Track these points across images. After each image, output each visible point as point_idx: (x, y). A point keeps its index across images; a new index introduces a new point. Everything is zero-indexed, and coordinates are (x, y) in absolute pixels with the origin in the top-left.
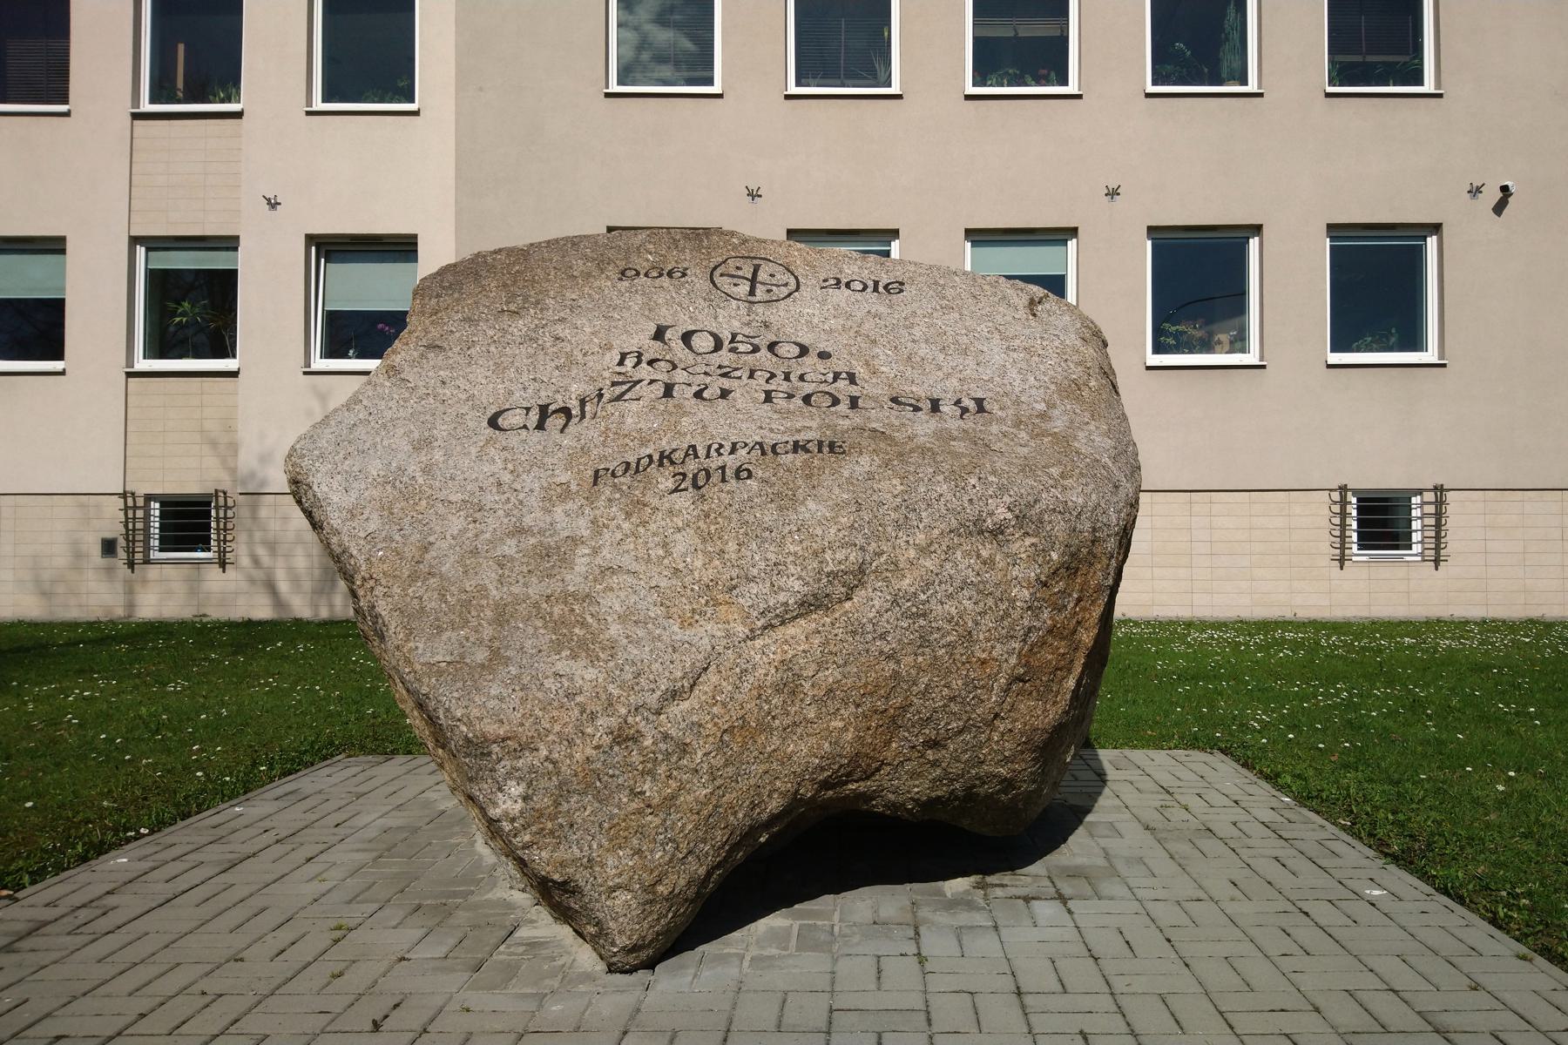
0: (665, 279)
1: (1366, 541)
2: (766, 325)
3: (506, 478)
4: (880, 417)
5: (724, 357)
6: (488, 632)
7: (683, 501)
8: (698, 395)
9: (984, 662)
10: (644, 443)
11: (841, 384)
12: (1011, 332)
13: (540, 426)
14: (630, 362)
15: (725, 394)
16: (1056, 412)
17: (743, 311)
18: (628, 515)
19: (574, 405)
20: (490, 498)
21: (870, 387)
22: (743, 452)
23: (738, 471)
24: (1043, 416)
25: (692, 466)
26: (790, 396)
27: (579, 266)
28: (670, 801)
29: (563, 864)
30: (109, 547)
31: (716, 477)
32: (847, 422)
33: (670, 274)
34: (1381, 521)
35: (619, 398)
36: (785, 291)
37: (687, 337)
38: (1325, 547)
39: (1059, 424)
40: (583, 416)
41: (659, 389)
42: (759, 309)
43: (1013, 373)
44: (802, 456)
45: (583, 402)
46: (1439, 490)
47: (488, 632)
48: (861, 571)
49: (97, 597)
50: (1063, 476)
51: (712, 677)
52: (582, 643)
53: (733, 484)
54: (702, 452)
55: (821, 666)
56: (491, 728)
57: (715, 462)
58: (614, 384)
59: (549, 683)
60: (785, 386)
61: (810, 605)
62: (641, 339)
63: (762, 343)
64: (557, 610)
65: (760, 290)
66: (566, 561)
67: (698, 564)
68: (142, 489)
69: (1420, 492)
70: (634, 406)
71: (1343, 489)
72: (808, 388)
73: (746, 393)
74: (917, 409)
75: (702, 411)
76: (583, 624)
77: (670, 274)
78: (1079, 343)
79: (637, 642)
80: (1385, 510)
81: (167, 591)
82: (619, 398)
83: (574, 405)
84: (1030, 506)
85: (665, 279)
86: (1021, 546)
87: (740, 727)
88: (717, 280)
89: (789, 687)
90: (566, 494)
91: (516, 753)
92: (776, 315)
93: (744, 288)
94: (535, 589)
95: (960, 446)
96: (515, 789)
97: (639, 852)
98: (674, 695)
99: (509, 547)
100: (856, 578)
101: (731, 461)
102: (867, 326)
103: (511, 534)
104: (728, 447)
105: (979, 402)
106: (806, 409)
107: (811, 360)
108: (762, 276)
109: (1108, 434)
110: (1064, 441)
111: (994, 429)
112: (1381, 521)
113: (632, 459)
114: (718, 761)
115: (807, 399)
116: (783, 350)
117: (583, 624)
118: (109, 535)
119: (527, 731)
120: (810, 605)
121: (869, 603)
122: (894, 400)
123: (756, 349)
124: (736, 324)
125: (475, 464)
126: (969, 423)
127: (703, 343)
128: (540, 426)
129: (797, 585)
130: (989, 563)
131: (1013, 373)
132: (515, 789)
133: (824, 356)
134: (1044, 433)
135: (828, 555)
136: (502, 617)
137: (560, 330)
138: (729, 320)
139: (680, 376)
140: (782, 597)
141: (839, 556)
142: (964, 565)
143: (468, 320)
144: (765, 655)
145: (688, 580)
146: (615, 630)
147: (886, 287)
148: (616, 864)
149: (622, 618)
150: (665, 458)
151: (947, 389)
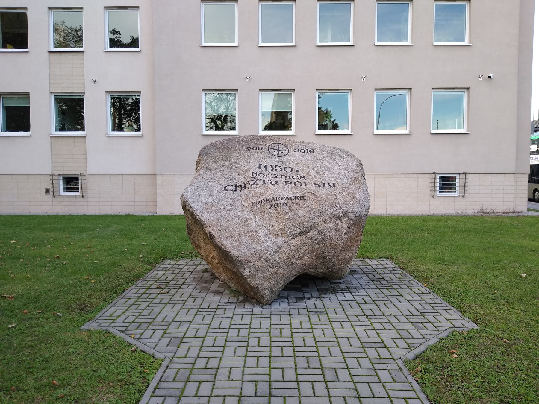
0: (257, 150)
1: (441, 190)
2: (283, 163)
3: (232, 203)
4: (313, 189)
5: (274, 172)
6: (237, 239)
7: (273, 210)
8: (271, 183)
9: (336, 245)
10: (261, 196)
11: (302, 179)
12: (340, 164)
13: (236, 190)
14: (255, 175)
15: (277, 182)
16: (351, 187)
17: (277, 159)
18: (261, 213)
19: (243, 185)
20: (229, 208)
21: (310, 181)
22: (284, 199)
23: (284, 204)
24: (348, 188)
25: (273, 202)
26: (291, 183)
27: (238, 147)
28: (276, 273)
29: (256, 284)
30: (47, 191)
31: (279, 206)
32: (305, 191)
33: (258, 149)
34: (447, 184)
35: (253, 184)
36: (286, 152)
37: (265, 167)
38: (428, 192)
39: (352, 190)
40: (245, 188)
41: (262, 182)
42: (281, 158)
43: (341, 176)
44: (297, 200)
45: (245, 184)
46: (465, 173)
47: (237, 239)
48: (312, 226)
49: (46, 206)
50: (353, 204)
51: (282, 249)
52: (257, 242)
53: (283, 207)
54: (275, 199)
55: (304, 246)
56: (244, 259)
57: (279, 202)
58: (252, 180)
59: (253, 250)
60: (289, 180)
61: (302, 233)
62: (256, 169)
63: (282, 168)
64: (251, 234)
65: (280, 152)
66: (249, 224)
67: (277, 225)
68: (57, 173)
69: (459, 174)
70: (258, 186)
71: (435, 173)
72: (295, 181)
73: (281, 184)
74: (320, 186)
75: (272, 188)
76: (257, 238)
77: (258, 149)
78: (356, 167)
79: (267, 241)
80: (448, 180)
81: (67, 205)
82: (253, 184)
83: (243, 185)
84: (346, 212)
85: (257, 150)
86: (345, 220)
87: (289, 259)
88: (270, 150)
89: (297, 250)
90: (246, 207)
91: (248, 263)
92: (284, 159)
93: (276, 152)
94: (245, 229)
95: (331, 197)
96: (248, 270)
97: (270, 282)
98: (276, 252)
99: (236, 220)
100: (312, 227)
101: (282, 202)
102: (306, 163)
103: (236, 217)
104: (281, 198)
105: (334, 184)
106: (295, 187)
107: (294, 172)
108: (280, 149)
109: (363, 192)
110: (353, 195)
111: (338, 192)
112: (447, 184)
113: (260, 200)
114: (284, 265)
115: (295, 183)
116: (287, 169)
117: (257, 238)
118: (47, 187)
119: (250, 259)
120: (302, 233)
121: (313, 233)
122: (314, 183)
123: (281, 170)
124: (276, 163)
125: (222, 199)
126: (332, 190)
127: (269, 168)
128: (236, 190)
129: (298, 230)
130: (338, 224)
131: (341, 176)
132: (248, 270)
133: (297, 171)
134: (349, 193)
135: (305, 223)
136: (239, 235)
137: (236, 165)
138: (274, 162)
139: (266, 178)
140: (296, 232)
141: (307, 223)
142: (332, 225)
143: (215, 162)
144: (293, 244)
145: (276, 228)
146: (263, 239)
147: (310, 151)
148: (267, 284)
149: (264, 236)
150: (267, 200)
151: (326, 180)
